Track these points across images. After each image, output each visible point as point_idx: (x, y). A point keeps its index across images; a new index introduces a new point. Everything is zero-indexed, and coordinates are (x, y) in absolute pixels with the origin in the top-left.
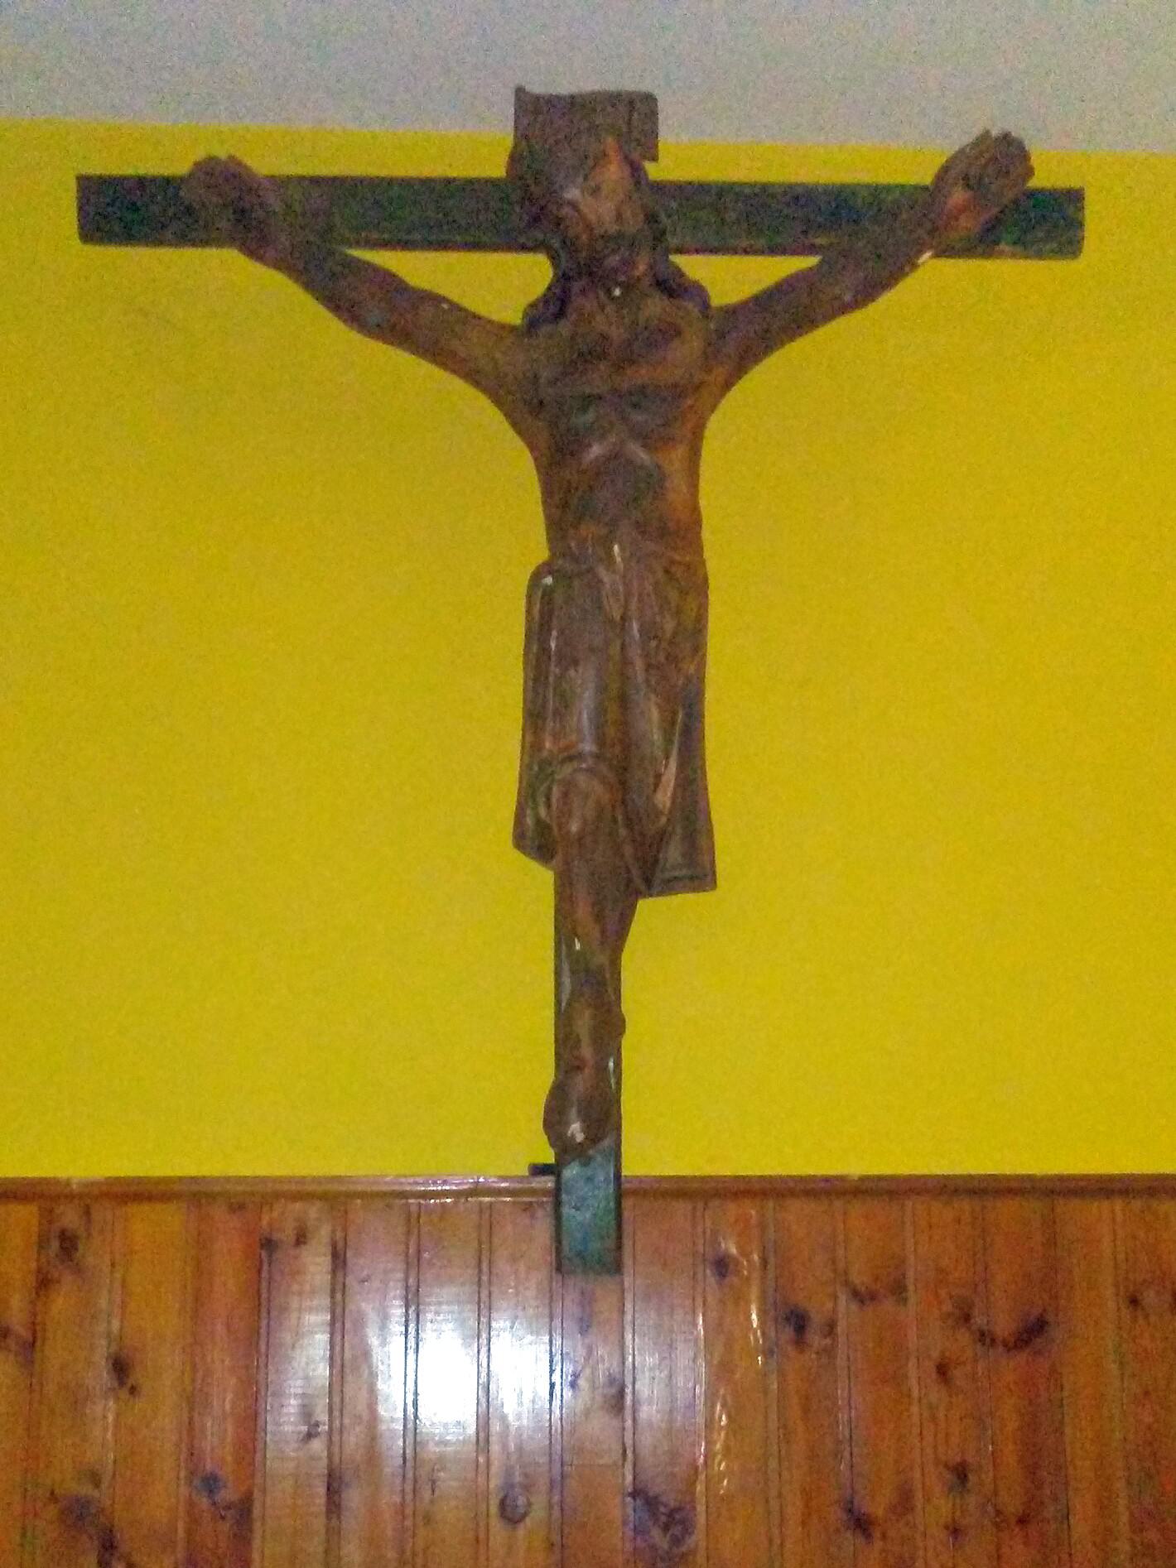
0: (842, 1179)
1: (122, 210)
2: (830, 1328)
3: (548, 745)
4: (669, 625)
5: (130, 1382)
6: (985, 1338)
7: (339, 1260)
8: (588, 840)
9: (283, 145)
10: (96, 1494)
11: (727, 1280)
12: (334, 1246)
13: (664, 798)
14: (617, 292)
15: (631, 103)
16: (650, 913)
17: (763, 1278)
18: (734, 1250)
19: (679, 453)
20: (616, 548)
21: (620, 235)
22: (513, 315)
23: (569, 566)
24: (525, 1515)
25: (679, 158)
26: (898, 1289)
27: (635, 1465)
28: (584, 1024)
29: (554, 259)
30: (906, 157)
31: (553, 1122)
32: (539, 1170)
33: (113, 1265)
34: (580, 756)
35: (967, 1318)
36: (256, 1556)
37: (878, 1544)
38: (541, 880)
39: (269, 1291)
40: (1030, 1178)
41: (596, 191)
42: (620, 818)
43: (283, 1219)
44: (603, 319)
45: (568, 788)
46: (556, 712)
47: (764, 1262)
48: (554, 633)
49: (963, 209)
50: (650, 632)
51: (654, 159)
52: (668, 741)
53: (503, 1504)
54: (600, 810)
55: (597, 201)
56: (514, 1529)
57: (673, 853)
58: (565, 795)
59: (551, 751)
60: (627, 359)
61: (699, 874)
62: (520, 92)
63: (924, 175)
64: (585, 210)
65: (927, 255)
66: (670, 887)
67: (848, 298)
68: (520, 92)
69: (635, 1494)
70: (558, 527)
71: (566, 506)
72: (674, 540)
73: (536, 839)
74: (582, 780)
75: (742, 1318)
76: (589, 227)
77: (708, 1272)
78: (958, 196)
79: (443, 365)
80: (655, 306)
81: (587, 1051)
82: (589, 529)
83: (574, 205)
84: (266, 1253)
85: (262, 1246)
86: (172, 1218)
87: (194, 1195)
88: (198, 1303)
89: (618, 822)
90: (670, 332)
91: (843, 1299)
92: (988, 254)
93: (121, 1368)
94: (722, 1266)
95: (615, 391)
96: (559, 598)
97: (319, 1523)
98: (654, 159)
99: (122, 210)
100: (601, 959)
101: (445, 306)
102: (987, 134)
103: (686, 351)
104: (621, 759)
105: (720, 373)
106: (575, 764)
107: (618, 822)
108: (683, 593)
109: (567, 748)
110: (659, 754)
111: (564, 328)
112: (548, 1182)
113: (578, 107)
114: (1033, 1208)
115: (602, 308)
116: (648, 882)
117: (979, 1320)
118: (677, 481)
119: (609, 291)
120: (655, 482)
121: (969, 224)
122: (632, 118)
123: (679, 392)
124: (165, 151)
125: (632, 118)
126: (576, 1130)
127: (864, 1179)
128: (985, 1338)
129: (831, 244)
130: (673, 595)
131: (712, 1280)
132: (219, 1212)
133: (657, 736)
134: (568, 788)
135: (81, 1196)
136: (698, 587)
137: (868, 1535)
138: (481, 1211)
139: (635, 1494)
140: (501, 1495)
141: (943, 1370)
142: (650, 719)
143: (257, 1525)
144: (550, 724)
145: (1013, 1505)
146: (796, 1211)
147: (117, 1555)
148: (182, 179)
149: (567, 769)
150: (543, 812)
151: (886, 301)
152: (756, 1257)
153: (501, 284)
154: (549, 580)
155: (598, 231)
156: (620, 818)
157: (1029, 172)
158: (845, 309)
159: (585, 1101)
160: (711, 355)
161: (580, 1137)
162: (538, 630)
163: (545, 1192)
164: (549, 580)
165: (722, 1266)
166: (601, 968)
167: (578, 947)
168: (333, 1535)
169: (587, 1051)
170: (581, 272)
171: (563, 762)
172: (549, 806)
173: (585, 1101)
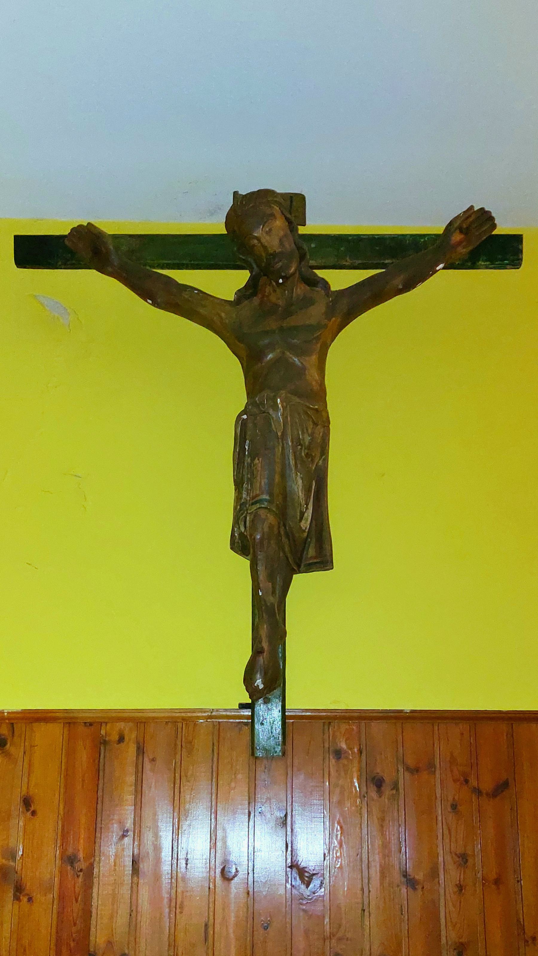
0: (401, 711)
1: (34, 252)
2: (395, 786)
3: (244, 496)
4: (307, 439)
5: (32, 809)
6: (478, 792)
7: (141, 751)
8: (266, 542)
9: (116, 221)
10: (12, 864)
11: (341, 761)
12: (138, 743)
13: (305, 524)
14: (281, 281)
15: (291, 197)
16: (300, 581)
17: (360, 762)
18: (344, 746)
19: (314, 358)
20: (279, 400)
21: (281, 253)
22: (231, 297)
23: (255, 410)
24: (234, 877)
25: (315, 224)
26: (431, 767)
27: (292, 851)
28: (264, 631)
29: (251, 272)
30: (430, 221)
31: (248, 680)
32: (243, 706)
33: (24, 753)
34: (260, 501)
35: (467, 781)
36: (95, 895)
37: (420, 892)
38: (244, 564)
39: (209, 908)
40: (500, 712)
41: (269, 233)
42: (282, 533)
43: (111, 732)
44: (276, 297)
45: (256, 515)
46: (249, 479)
47: (360, 752)
48: (248, 442)
49: (459, 243)
50: (298, 442)
51: (304, 224)
52: (307, 498)
53: (223, 870)
54: (271, 527)
55: (270, 236)
56: (229, 883)
57: (311, 552)
58: (253, 521)
59: (245, 499)
60: (288, 313)
61: (324, 562)
62: (235, 193)
63: (439, 229)
64: (263, 241)
65: (441, 266)
66: (310, 568)
67: (401, 287)
68: (235, 193)
69: (291, 867)
70: (250, 394)
71: (255, 383)
72: (312, 404)
73: (241, 544)
74: (262, 512)
75: (349, 780)
76: (265, 248)
77: (331, 757)
78: (457, 237)
79: (137, 235)
80: (300, 290)
81: (265, 645)
82: (266, 393)
83: (258, 239)
84: (100, 744)
85: (101, 743)
86: (56, 730)
87: (69, 720)
88: (68, 776)
89: (283, 534)
90: (307, 302)
91: (401, 769)
92: (474, 266)
93: (27, 802)
94: (338, 754)
95: (281, 329)
96: (250, 425)
97: (128, 879)
98: (304, 224)
99: (34, 252)
100: (272, 600)
101: (196, 292)
102: (472, 207)
103: (316, 312)
104: (284, 508)
105: (335, 320)
106: (258, 505)
107: (283, 534)
108: (315, 424)
109: (253, 498)
110: (303, 502)
111: (256, 300)
112: (247, 713)
113: (263, 196)
114: (504, 727)
115: (275, 291)
116: (299, 566)
117: (473, 782)
118: (312, 374)
119: (277, 282)
120: (301, 372)
121: (463, 251)
122: (293, 206)
123: (311, 328)
124: (57, 224)
125: (293, 206)
126: (259, 683)
127: (413, 711)
128: (478, 792)
129: (392, 263)
130: (310, 425)
131: (333, 761)
132: (81, 729)
133: (301, 494)
134: (256, 515)
135: (9, 719)
136: (322, 422)
137: (415, 889)
138: (214, 725)
139: (291, 867)
140: (221, 867)
141: (454, 807)
142: (297, 485)
143: (95, 881)
144: (245, 485)
145: (493, 876)
146: (376, 727)
147: (23, 893)
148: (65, 236)
149: (255, 507)
150: (243, 529)
151: (420, 288)
152: (356, 750)
153: (225, 284)
154: (245, 417)
155: (271, 251)
156: (282, 533)
157: (494, 226)
158: (400, 292)
159: (266, 672)
160: (331, 311)
161: (261, 686)
162: (240, 440)
163: (247, 717)
164: (245, 417)
165: (338, 754)
166: (273, 605)
167: (260, 594)
168: (134, 887)
169: (265, 645)
170: (264, 273)
171: (253, 504)
172: (245, 527)
173: (266, 672)
